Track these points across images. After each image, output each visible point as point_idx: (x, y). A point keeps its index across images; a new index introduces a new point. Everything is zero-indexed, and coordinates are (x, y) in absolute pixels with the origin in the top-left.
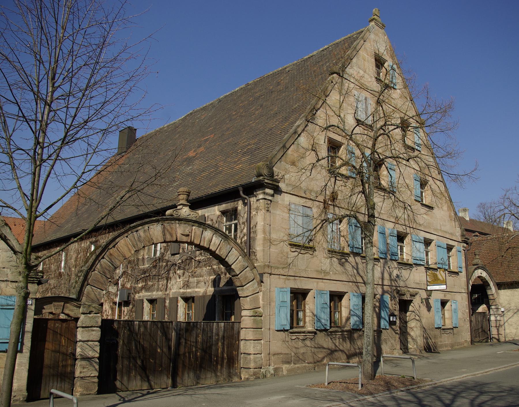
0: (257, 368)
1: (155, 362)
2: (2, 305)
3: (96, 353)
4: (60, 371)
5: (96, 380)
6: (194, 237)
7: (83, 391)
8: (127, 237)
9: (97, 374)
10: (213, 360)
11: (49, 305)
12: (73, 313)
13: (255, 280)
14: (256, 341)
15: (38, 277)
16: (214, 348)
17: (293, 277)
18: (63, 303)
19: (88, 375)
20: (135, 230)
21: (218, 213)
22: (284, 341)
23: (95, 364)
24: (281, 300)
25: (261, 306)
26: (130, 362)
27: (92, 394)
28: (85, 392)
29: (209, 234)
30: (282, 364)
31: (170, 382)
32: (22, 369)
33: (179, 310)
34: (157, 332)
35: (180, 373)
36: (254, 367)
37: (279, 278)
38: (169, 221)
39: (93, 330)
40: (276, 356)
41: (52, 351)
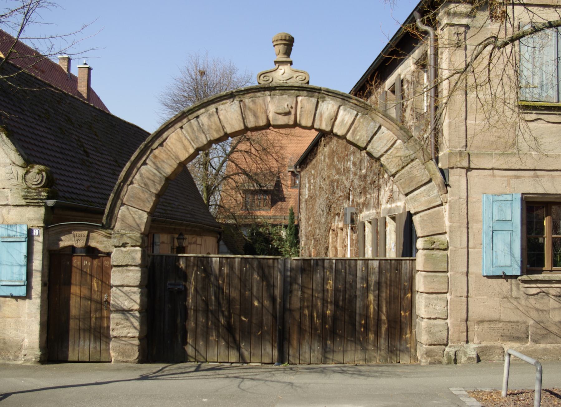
0: (435, 345)
1: (250, 322)
2: (2, 237)
3: (134, 303)
4: (92, 325)
5: (137, 342)
6: (301, 115)
7: (118, 356)
8: (181, 128)
9: (137, 334)
10: (357, 324)
11: (67, 236)
12: (103, 246)
13: (433, 183)
14: (434, 295)
15: (42, 197)
16: (359, 303)
17: (532, 173)
18: (86, 233)
19: (123, 335)
20: (195, 114)
21: (413, 67)
22: (506, 297)
23: (133, 320)
24: (495, 218)
25: (447, 230)
26: (207, 319)
27: (131, 362)
28: (120, 358)
29: (330, 106)
30: (504, 340)
31: (276, 353)
32: (32, 321)
33: (388, 237)
34: (252, 275)
35: (295, 343)
36: (427, 342)
37: (494, 176)
38: (252, 95)
39: (130, 270)
40: (486, 325)
41: (81, 297)
